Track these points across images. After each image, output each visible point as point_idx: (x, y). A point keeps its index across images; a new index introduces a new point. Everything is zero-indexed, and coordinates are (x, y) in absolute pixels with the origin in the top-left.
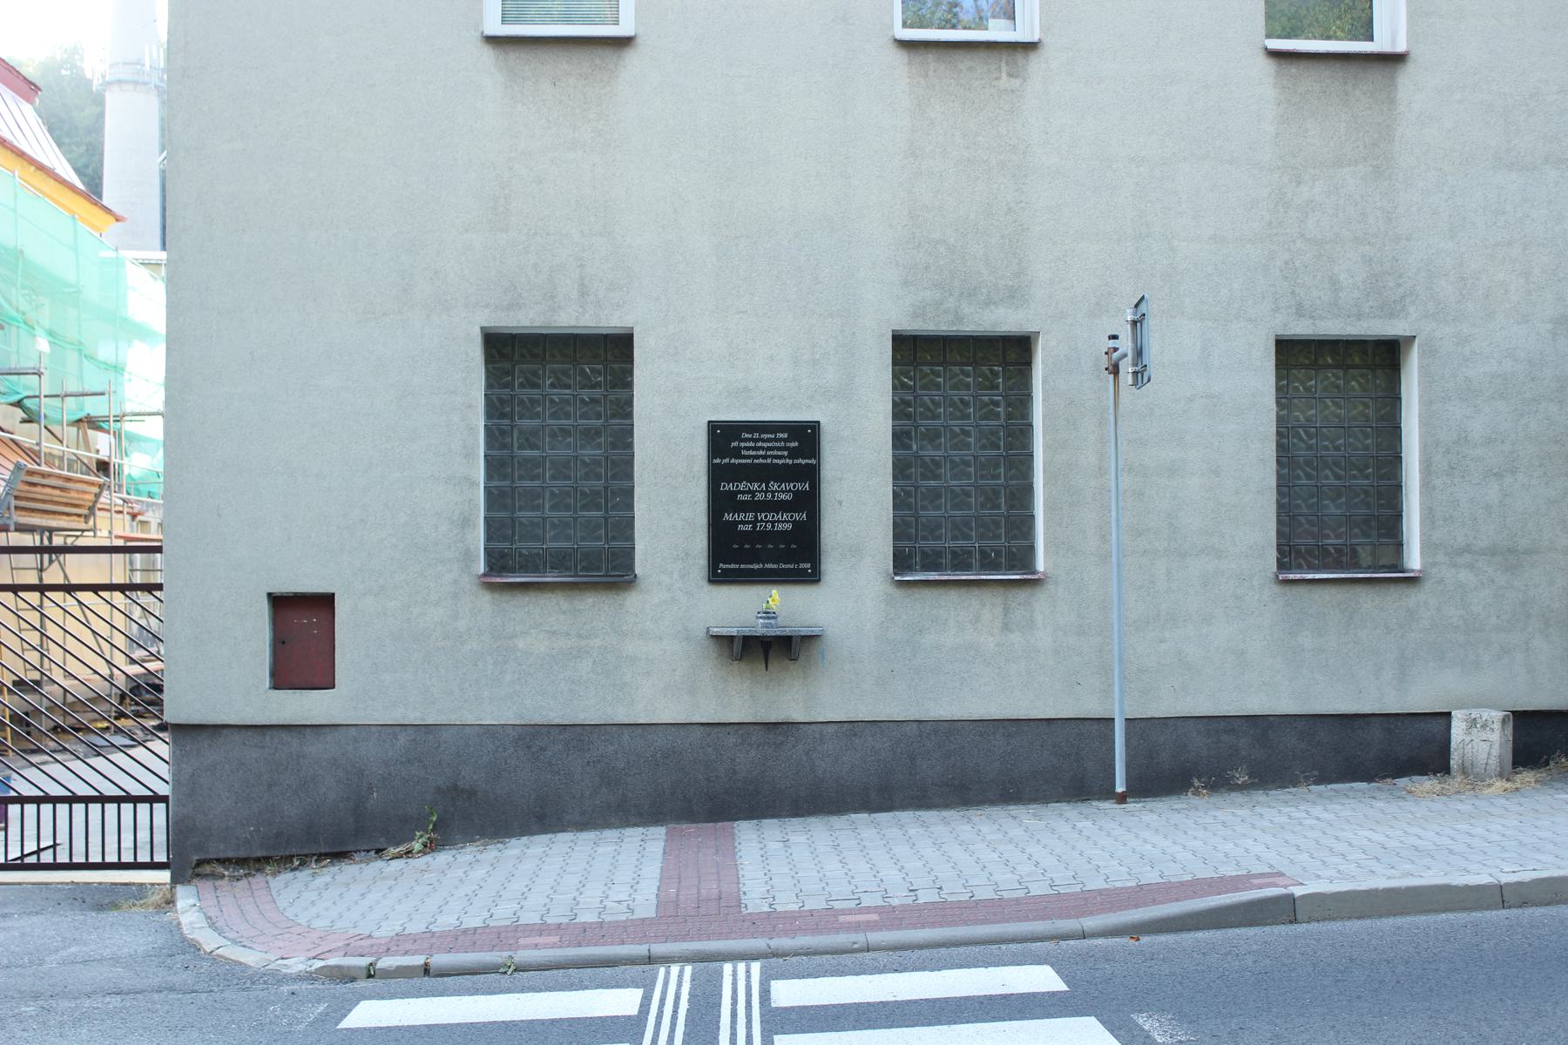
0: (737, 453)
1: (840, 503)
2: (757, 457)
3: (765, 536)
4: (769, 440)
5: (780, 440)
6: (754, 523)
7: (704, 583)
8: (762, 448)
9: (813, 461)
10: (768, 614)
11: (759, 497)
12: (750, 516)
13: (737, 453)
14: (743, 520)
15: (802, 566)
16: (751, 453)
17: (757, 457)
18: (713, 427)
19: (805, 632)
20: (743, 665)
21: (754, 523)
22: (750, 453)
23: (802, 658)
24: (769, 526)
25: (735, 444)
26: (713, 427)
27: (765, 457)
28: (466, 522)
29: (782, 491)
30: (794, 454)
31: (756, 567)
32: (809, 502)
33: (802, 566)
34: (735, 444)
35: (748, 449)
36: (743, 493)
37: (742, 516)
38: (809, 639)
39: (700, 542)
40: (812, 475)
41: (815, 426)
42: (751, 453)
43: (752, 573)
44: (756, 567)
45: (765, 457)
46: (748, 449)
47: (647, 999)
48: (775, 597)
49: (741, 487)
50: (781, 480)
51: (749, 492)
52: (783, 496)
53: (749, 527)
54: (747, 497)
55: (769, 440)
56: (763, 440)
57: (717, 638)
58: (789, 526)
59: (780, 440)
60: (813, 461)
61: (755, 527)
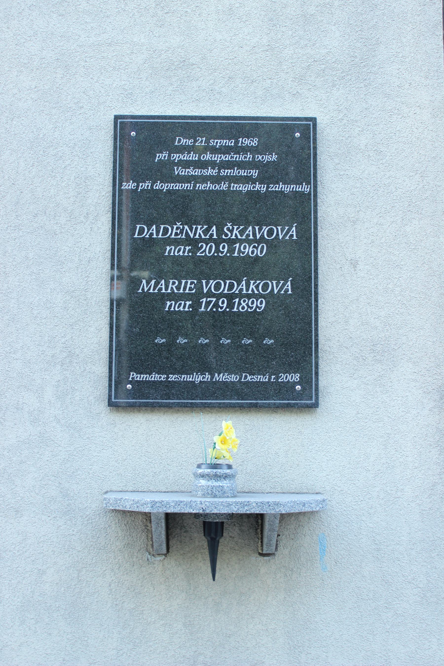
0: (164, 172)
1: (354, 264)
2: (204, 179)
3: (221, 322)
4: (226, 150)
5: (245, 150)
6: (196, 298)
7: (103, 406)
8: (213, 164)
9: (305, 188)
10: (217, 469)
11: (206, 250)
12: (188, 285)
13: (164, 172)
14: (176, 293)
15: (285, 378)
16: (191, 171)
17: (204, 179)
18: (123, 126)
19: (287, 503)
20: (171, 563)
21: (196, 298)
22: (192, 171)
23: (283, 551)
24: (224, 304)
25: (163, 156)
26: (123, 126)
27: (217, 180)
28: (220, 570)
29: (247, 242)
30: (268, 174)
31: (198, 378)
32: (299, 264)
33: (285, 378)
34: (163, 156)
35: (186, 164)
36: (176, 242)
37: (173, 285)
38: (312, 513)
39: (93, 337)
40: (303, 212)
41: (307, 128)
42: (191, 171)
43: (190, 390)
44: (198, 378)
45: (217, 180)
46: (186, 164)
47: (121, 185)
48: (228, 434)
49: (172, 232)
50: (242, 220)
51: (189, 241)
52: (248, 250)
53: (185, 306)
54: (183, 251)
55: (226, 150)
56: (214, 150)
57: (127, 515)
58: (260, 305)
59: (245, 150)
60: (305, 188)
61: (196, 304)
